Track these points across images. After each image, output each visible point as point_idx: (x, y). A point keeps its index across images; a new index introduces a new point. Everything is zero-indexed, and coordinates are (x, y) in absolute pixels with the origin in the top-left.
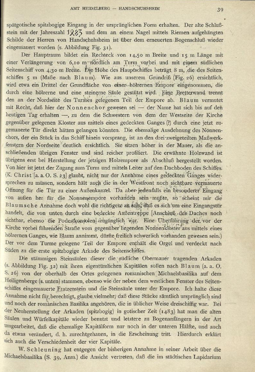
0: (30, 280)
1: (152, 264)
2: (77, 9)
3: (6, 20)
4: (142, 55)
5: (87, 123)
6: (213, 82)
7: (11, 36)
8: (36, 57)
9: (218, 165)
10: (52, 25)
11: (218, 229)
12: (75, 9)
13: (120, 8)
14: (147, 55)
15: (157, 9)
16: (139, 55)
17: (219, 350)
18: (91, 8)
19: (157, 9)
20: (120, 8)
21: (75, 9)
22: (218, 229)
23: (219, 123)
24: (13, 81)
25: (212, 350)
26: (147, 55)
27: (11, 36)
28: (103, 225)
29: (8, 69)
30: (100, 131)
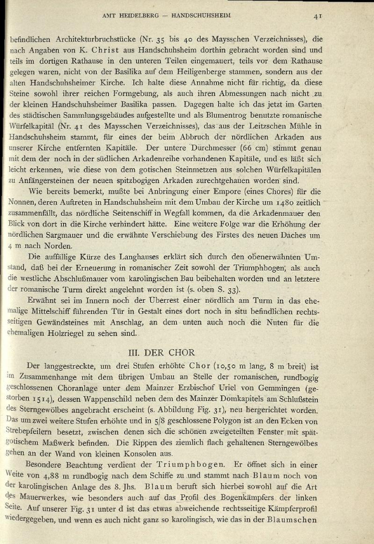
0: (57, 507)
1: (252, 436)
2: (112, 16)
3: (11, 31)
4: (234, 366)
5: (146, 432)
6: (312, 121)
7: (17, 89)
8: (55, 108)
9: (318, 110)
10: (137, 181)
11: (315, 149)
12: (109, 16)
13: (173, 15)
14: (242, 367)
15: (229, 16)
16: (230, 366)
17: (318, 192)
18: (216, 15)
19: (229, 16)
20: (173, 15)
21: (109, 16)
22: (315, 149)
23: (318, 94)
24: (18, 218)
25: (308, 193)
26: (242, 367)
27: (17, 89)
28: (168, 285)
29: (11, 170)
30: (173, 520)
